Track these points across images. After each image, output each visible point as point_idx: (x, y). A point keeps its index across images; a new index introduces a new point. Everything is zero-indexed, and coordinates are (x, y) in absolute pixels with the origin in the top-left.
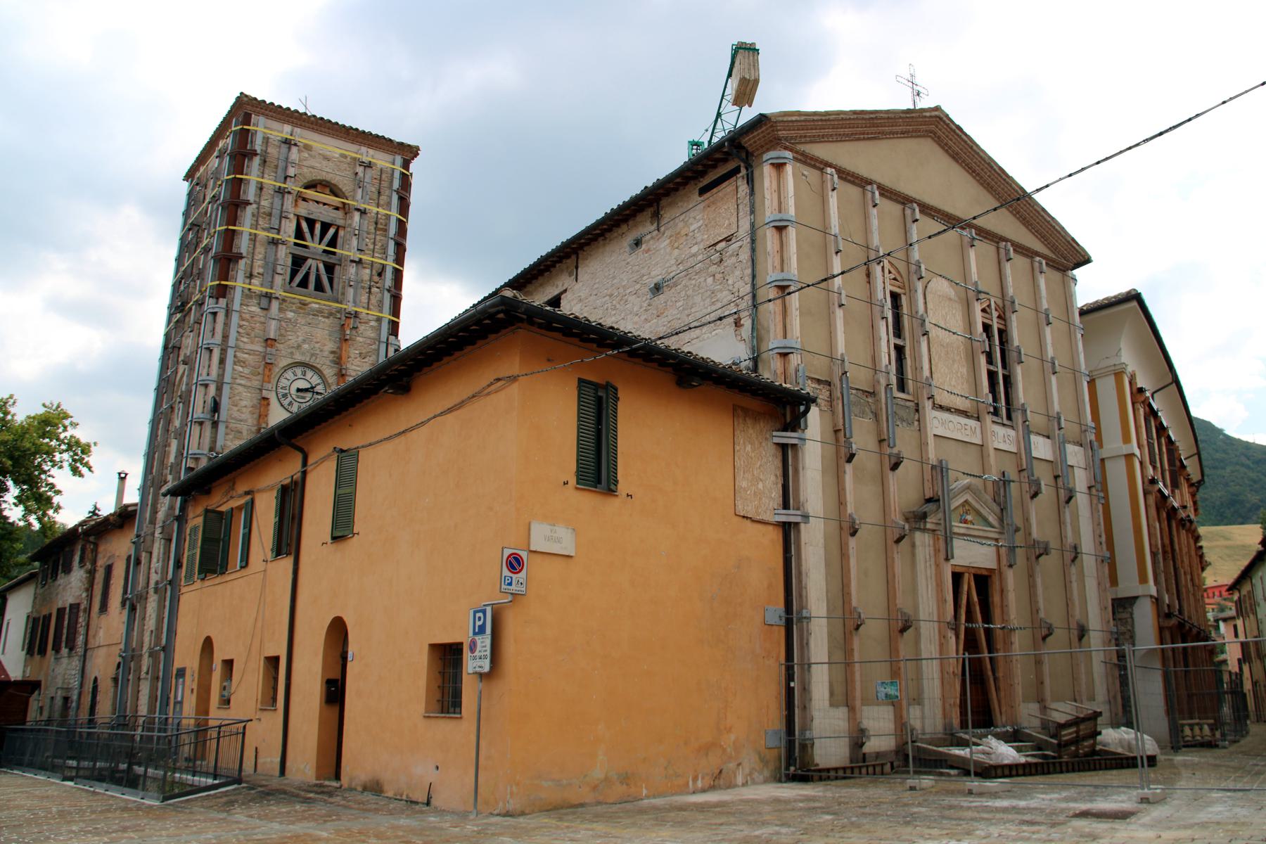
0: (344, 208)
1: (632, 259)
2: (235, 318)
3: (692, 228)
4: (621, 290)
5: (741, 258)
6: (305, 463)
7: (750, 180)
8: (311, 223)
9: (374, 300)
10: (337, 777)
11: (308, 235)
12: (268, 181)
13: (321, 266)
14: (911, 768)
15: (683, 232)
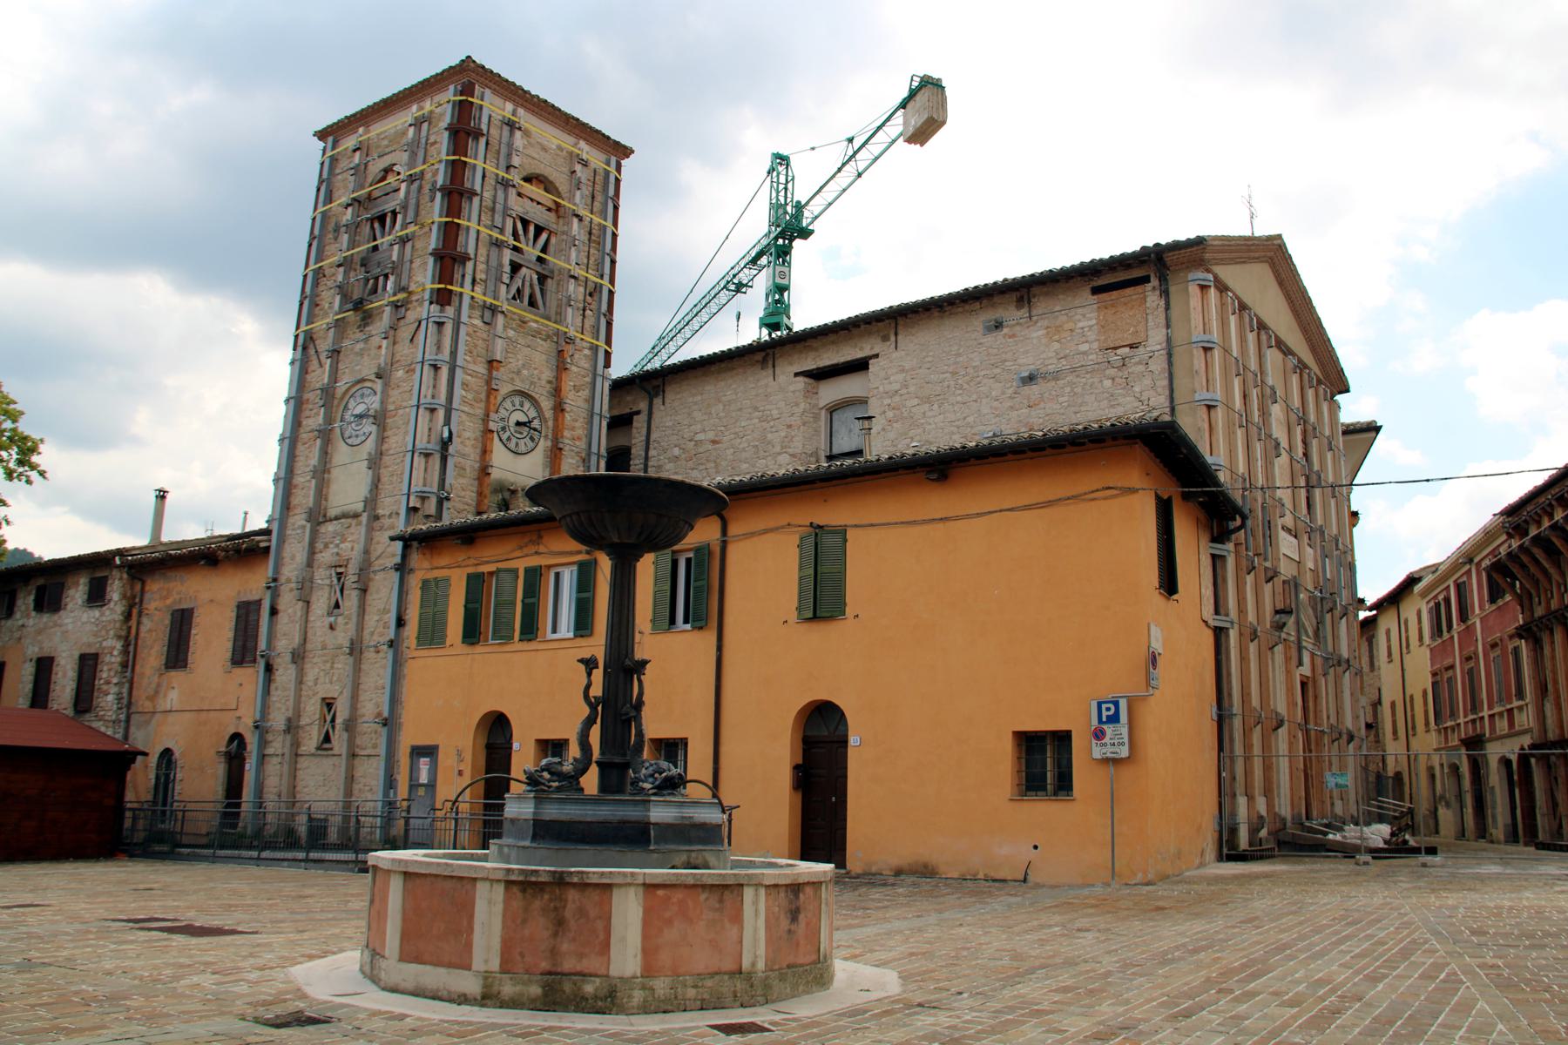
0: (556, 209)
1: (989, 339)
2: (463, 330)
3: (1081, 325)
4: (970, 370)
5: (1152, 367)
6: (724, 532)
7: (1165, 294)
8: (525, 223)
9: (589, 322)
10: (1437, 832)
11: (522, 238)
12: (490, 168)
13: (535, 277)
14: (1521, 839)
15: (1068, 326)
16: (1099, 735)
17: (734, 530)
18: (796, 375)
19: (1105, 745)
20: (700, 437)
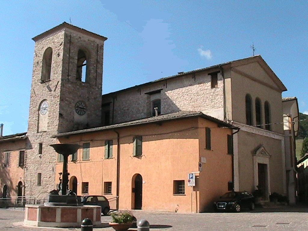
16: (189, 181)
17: (121, 136)
18: (145, 94)
19: (190, 183)
20: (125, 108)
